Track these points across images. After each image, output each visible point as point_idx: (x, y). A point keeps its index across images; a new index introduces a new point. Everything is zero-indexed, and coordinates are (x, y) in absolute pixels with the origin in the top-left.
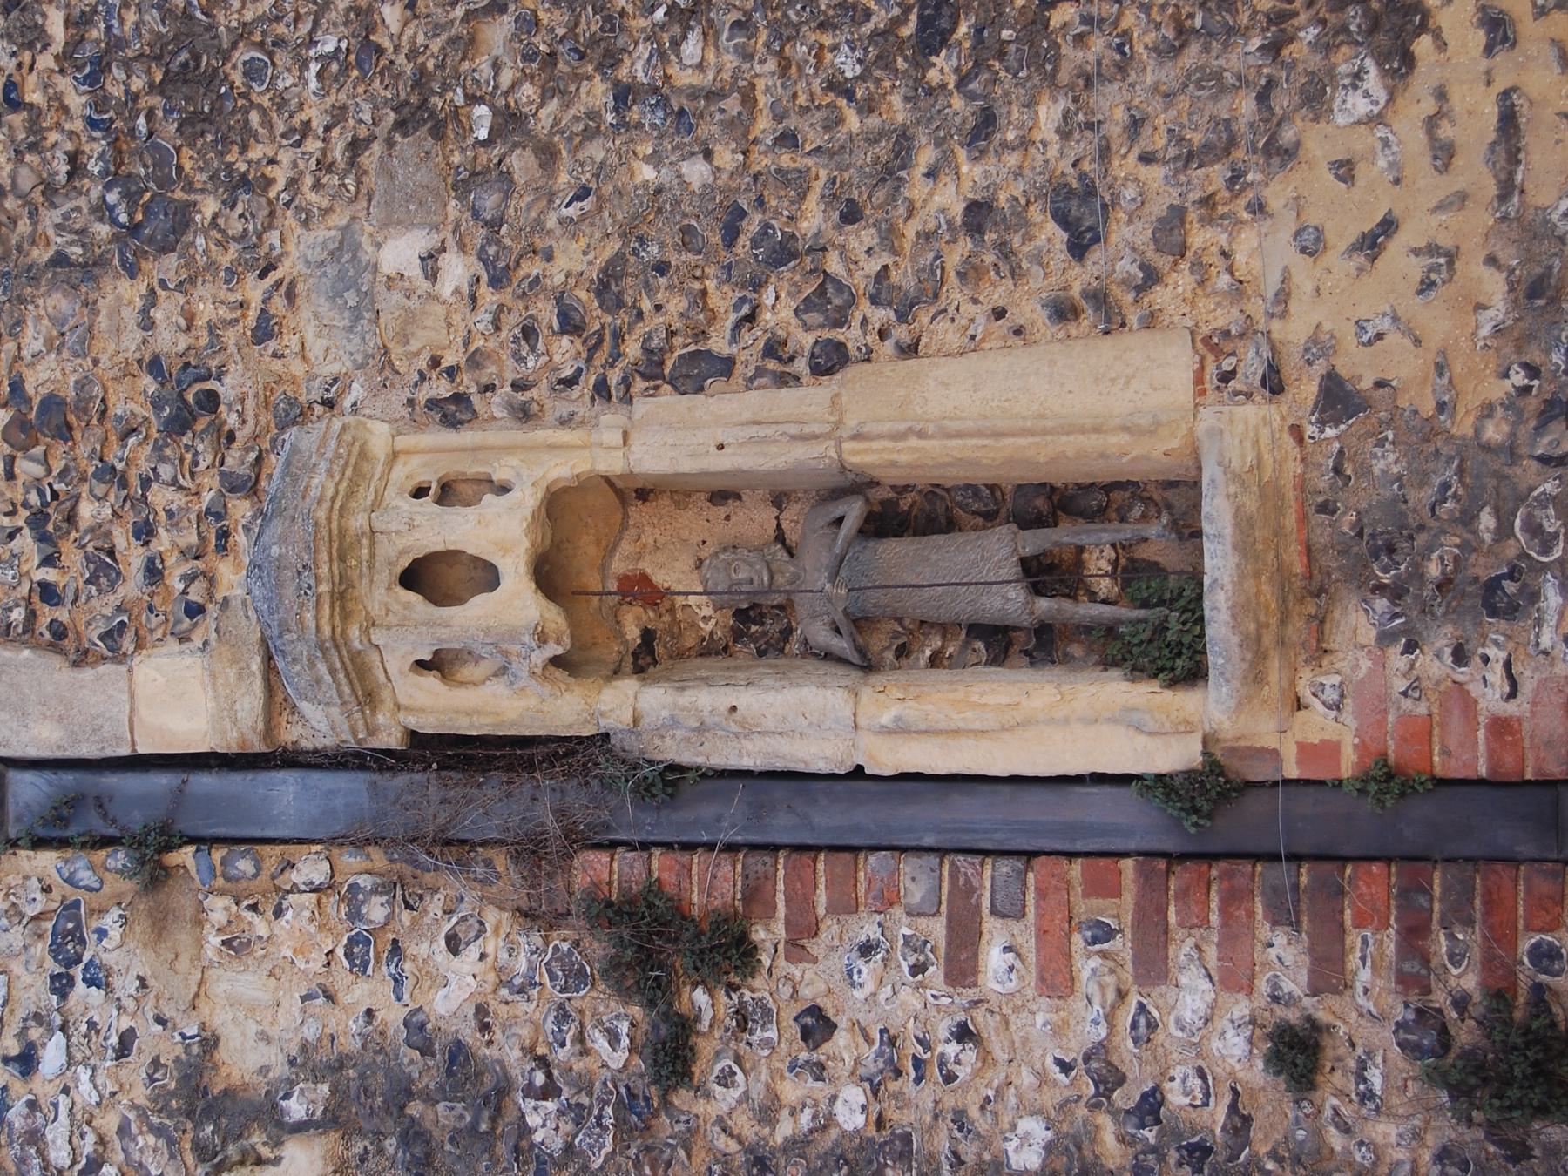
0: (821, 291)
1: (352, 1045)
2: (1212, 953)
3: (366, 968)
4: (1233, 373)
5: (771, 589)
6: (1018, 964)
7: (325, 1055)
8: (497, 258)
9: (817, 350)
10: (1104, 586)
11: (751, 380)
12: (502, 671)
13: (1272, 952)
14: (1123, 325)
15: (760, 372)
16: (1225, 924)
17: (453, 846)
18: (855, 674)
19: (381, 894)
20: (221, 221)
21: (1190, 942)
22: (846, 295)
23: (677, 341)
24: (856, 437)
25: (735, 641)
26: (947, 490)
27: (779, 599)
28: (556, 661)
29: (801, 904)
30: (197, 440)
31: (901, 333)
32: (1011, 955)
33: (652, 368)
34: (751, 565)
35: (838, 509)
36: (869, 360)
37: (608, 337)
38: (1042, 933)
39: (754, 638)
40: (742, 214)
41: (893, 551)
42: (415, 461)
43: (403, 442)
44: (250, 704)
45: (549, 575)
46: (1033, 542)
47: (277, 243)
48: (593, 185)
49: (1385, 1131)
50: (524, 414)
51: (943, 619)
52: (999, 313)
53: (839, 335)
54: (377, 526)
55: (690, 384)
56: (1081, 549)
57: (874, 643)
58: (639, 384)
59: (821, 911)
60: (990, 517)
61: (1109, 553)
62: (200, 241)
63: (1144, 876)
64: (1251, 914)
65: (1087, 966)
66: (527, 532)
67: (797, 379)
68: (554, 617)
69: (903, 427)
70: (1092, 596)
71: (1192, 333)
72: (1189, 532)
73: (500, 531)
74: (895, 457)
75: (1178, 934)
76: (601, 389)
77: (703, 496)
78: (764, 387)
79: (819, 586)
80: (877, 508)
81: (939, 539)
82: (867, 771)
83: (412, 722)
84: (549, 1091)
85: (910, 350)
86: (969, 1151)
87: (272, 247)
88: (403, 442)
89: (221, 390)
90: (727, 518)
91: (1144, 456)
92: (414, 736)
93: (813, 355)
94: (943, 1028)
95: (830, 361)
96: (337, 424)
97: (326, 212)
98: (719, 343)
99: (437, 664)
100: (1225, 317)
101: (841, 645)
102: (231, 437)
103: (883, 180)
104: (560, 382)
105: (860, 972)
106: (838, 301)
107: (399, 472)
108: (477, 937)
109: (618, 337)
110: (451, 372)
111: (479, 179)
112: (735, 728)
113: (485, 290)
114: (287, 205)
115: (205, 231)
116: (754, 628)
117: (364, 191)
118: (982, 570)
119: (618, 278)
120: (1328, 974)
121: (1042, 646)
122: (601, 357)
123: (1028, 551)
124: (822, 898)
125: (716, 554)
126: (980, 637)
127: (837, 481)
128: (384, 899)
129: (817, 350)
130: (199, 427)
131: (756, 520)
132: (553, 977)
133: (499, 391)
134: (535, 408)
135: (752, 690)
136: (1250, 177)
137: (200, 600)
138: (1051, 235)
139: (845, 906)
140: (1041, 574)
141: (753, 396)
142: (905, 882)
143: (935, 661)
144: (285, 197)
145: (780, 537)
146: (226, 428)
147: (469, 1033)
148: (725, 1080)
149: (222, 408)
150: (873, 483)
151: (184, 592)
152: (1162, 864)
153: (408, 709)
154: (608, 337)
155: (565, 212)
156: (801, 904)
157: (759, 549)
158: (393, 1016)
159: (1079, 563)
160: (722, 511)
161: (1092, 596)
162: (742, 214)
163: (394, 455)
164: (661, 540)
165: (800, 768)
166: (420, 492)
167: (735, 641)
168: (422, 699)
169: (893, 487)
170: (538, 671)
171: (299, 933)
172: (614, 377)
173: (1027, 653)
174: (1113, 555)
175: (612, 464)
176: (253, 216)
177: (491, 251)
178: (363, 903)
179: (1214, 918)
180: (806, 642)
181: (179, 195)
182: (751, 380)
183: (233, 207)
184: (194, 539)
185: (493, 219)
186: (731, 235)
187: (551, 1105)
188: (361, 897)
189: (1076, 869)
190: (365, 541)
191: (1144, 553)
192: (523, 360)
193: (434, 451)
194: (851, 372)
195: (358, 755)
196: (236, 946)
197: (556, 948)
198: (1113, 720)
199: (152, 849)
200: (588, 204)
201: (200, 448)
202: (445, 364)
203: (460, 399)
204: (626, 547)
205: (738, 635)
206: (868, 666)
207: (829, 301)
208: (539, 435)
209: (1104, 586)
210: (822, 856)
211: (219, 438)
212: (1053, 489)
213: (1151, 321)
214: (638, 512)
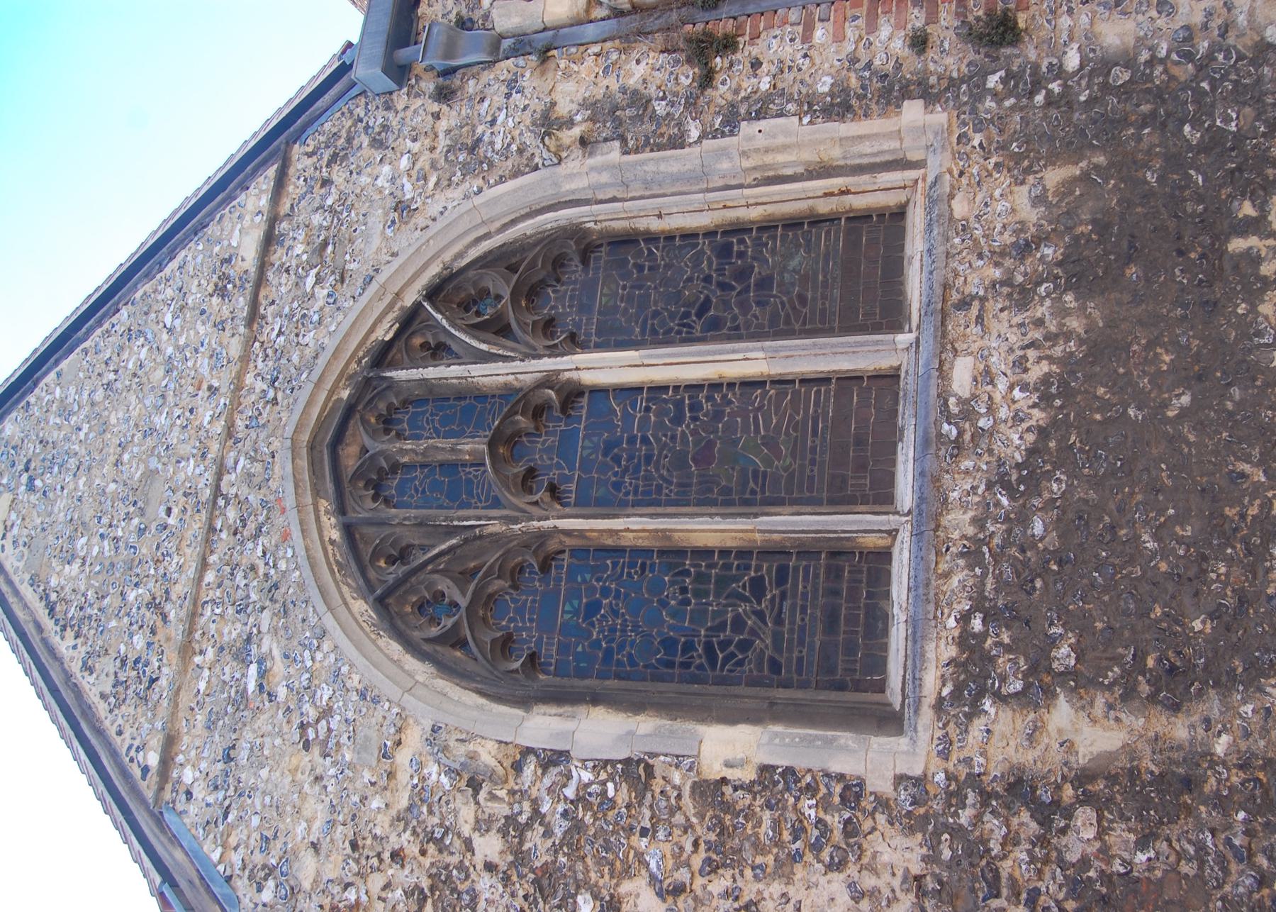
1: (600, 97)
2: (892, 20)
7: (592, 100)
17: (642, 33)
29: (755, 26)
49: (949, 60)
65: (849, 33)
75: (881, 15)
84: (663, 99)
86: (804, 91)
94: (799, 55)
120: (932, 18)
147: (640, 87)
148: (723, 83)
156: (755, 26)
158: (615, 87)
171: (588, 67)
187: (664, 103)
196: (567, 75)
199: (544, 55)
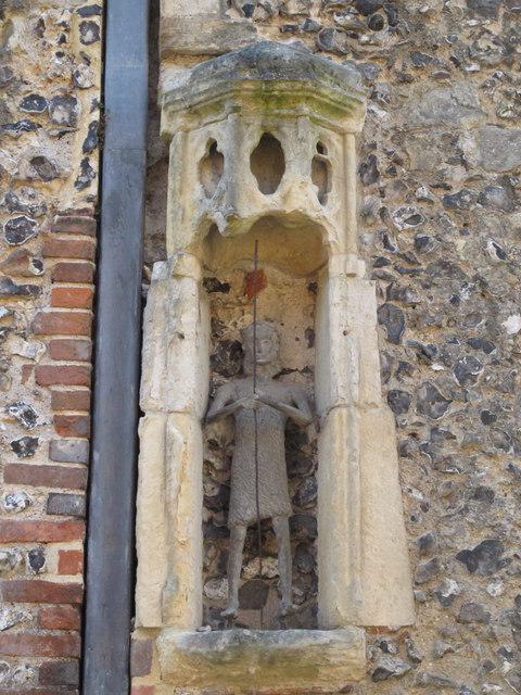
0: (440, 398)
3: (25, 107)
4: (386, 651)
5: (255, 363)
6: (18, 509)
8: (462, 201)
9: (404, 395)
10: (252, 570)
11: (386, 354)
12: (208, 195)
13: (23, 668)
14: (417, 584)
15: (390, 359)
16: (41, 638)
18: (200, 414)
19: (70, 118)
20: (486, 35)
21: (30, 617)
22: (437, 413)
23: (410, 310)
24: (350, 417)
25: (221, 342)
26: (313, 475)
27: (248, 369)
28: (214, 227)
30: (353, 16)
31: (413, 446)
32: (23, 504)
33: (393, 294)
34: (269, 352)
35: (303, 404)
36: (397, 426)
37: (413, 267)
38: (37, 524)
39: (222, 353)
40: (488, 350)
41: (276, 444)
42: (339, 147)
43: (351, 140)
44: (190, 41)
45: (270, 223)
46: (281, 526)
47: (472, 68)
48: (506, 261)
50: (365, 215)
51: (234, 470)
52: (425, 508)
53: (413, 409)
54: (301, 120)
55: (384, 318)
56: (275, 556)
57: (223, 433)
58: (384, 285)
59: (54, 388)
60: (296, 500)
61: (272, 574)
62: (474, 22)
63: (72, 588)
64: (46, 654)
66: (296, 211)
67: (386, 382)
68: (246, 226)
69: (356, 446)
70: (246, 562)
71: (411, 626)
72: (287, 621)
73: (298, 192)
74: (338, 441)
76: (381, 262)
77: (312, 325)
78: (381, 362)
79: (258, 391)
80: (302, 430)
81: (283, 468)
82: (141, 419)
83: (178, 139)
85: (403, 452)
87: (469, 65)
88: (351, 140)
89: (383, 32)
90: (297, 339)
91: (335, 595)
92: (168, 139)
93: (401, 392)
95: (395, 401)
96: (364, 99)
97: (491, 98)
98: (409, 335)
99: (213, 155)
100: (422, 648)
101: (219, 405)
102: (355, 36)
103: (508, 438)
104: (386, 236)
105: (15, 411)
106: (433, 408)
107: (335, 138)
108: (42, 176)
109: (413, 273)
110: (392, 171)
111: (510, 190)
112: (170, 337)
113: (441, 193)
114: (495, 76)
115: (480, 25)
116: (228, 354)
117: (504, 122)
118: (262, 495)
119: (450, 273)
121: (216, 530)
122: (401, 263)
123: (276, 522)
124: (61, 389)
125: (276, 331)
126: (220, 494)
127: (322, 406)
128: (67, 120)
129: (404, 395)
130: (361, 18)
131: (297, 357)
132: (16, 221)
133: (380, 200)
134: (370, 221)
135: (194, 349)
136: (506, 663)
137: (254, 15)
138: (469, 542)
139: (57, 402)
140: (260, 533)
141: (376, 355)
142: (72, 440)
143: (206, 463)
144: (500, 74)
145: (285, 372)
146: (360, 34)
149: (372, 32)
150: (319, 429)
151: (259, 5)
152: (79, 600)
153: (185, 138)
154: (413, 267)
155: (490, 243)
157: (278, 358)
159: (266, 554)
160: (302, 336)
161: (246, 562)
162: (488, 350)
163: (343, 134)
164: (285, 298)
165: (143, 378)
166: (320, 148)
167: (221, 342)
168: (191, 146)
169: (316, 441)
170: (209, 217)
172: (388, 270)
173: (211, 520)
174: (270, 576)
175: (336, 266)
176: (488, 55)
177: (467, 198)
178: (65, 106)
179: (44, 633)
180: (219, 385)
181: (502, 11)
182: (386, 354)
183: (494, 43)
184: (292, 12)
185: (486, 199)
186: (474, 344)
188: (69, 105)
189: (77, 546)
190: (292, 112)
191: (272, 594)
192: (399, 215)
193: (345, 157)
194: (390, 414)
195: (156, 92)
197: (34, 224)
198: (170, 572)
200: (495, 257)
201: (348, 18)
202: (398, 167)
203: (376, 175)
204: (280, 276)
205: (225, 344)
206: (205, 422)
207: (438, 398)
208: (354, 222)
209: (252, 570)
210: (86, 389)
211: (353, 29)
212: (313, 540)
213: (419, 602)
214: (302, 282)
